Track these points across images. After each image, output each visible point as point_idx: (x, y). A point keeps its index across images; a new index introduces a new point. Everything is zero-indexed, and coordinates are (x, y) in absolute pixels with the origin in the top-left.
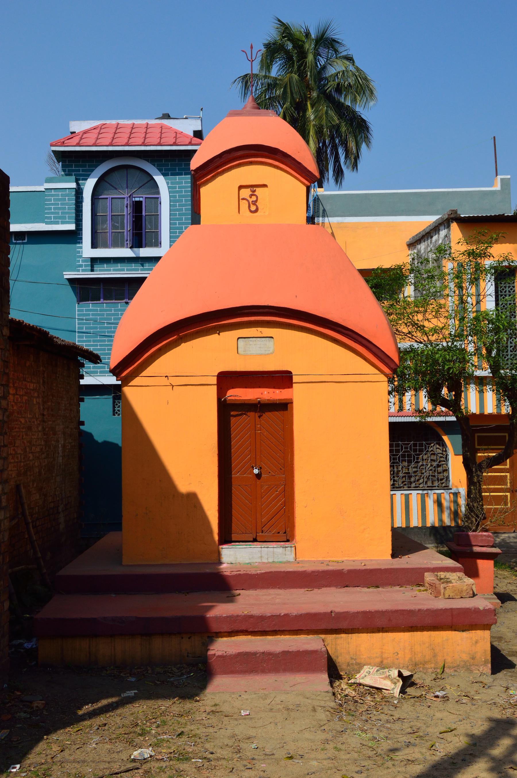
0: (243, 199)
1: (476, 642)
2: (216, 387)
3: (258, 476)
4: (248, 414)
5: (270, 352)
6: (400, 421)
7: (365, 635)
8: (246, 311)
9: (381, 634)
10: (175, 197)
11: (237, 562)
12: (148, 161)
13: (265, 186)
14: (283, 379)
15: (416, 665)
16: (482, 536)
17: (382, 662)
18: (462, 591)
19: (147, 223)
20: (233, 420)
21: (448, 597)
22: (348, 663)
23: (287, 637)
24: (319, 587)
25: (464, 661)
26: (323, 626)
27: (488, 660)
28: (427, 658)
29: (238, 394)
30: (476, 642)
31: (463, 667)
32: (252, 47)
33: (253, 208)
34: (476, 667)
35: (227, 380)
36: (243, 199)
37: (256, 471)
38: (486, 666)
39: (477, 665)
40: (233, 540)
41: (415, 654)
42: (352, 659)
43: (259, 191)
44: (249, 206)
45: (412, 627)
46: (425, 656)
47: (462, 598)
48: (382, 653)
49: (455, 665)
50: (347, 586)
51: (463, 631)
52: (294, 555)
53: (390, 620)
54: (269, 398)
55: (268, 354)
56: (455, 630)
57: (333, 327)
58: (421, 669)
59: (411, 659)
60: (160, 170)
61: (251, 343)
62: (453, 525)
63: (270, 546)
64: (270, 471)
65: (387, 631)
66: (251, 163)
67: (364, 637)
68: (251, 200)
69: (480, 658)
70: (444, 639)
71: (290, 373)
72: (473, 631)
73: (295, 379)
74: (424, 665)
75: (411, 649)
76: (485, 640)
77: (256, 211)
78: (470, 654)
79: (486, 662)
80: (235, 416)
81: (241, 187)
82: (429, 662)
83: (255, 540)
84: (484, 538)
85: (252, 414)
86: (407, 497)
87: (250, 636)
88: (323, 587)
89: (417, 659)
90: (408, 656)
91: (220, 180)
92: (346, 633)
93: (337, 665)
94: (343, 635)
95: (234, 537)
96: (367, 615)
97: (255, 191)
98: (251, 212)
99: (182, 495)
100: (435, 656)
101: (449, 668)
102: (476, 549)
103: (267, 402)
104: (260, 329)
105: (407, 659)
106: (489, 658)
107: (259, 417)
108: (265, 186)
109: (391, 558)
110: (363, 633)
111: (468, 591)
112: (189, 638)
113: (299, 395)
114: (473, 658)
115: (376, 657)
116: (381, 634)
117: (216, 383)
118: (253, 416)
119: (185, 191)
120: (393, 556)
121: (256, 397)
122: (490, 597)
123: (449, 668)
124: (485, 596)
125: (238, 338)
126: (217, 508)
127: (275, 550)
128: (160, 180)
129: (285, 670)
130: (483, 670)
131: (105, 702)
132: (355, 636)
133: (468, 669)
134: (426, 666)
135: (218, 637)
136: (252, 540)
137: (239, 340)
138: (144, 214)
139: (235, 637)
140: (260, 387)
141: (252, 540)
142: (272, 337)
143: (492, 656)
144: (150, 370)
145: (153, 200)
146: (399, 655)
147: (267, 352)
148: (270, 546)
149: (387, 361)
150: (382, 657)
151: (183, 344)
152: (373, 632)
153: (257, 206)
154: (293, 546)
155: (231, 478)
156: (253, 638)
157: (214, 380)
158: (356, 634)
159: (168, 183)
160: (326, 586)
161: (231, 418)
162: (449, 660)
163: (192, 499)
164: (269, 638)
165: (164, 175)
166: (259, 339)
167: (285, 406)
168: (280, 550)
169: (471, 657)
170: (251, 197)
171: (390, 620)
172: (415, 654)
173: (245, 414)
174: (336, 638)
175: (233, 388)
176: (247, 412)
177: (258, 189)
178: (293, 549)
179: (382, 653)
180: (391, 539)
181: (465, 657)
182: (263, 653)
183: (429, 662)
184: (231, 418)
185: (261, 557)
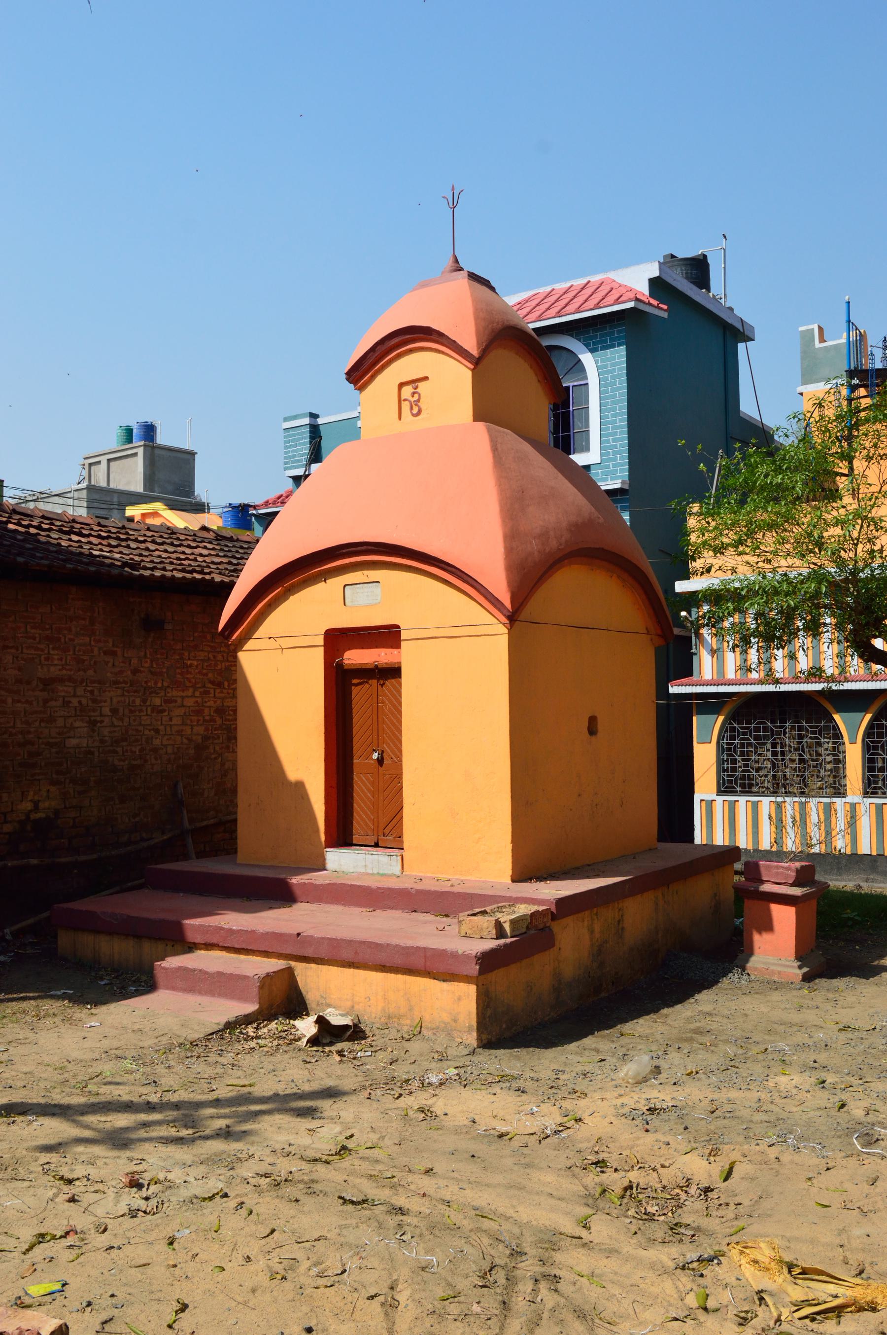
0: (405, 400)
1: (459, 999)
4: (370, 681)
5: (377, 601)
7: (335, 968)
10: (606, 379)
12: (572, 336)
14: (389, 635)
15: (389, 1017)
16: (777, 867)
17: (353, 1007)
19: (576, 420)
20: (355, 690)
25: (444, 1023)
29: (355, 657)
30: (459, 999)
31: (443, 1031)
32: (453, 189)
33: (415, 411)
35: (337, 640)
36: (405, 400)
42: (322, 997)
43: (421, 385)
44: (411, 408)
45: (384, 966)
48: (353, 995)
49: (434, 1026)
51: (444, 981)
53: (356, 953)
55: (376, 604)
59: (384, 1009)
60: (587, 345)
61: (358, 591)
65: (358, 968)
66: (411, 351)
68: (412, 400)
71: (398, 627)
72: (456, 983)
73: (404, 635)
74: (399, 1019)
77: (419, 412)
78: (451, 1013)
79: (470, 1027)
81: (401, 385)
83: (376, 845)
84: (781, 870)
85: (374, 682)
86: (755, 806)
89: (391, 1010)
91: (380, 379)
94: (313, 966)
95: (356, 839)
96: (335, 943)
97: (416, 388)
98: (414, 415)
99: (290, 783)
100: (411, 1009)
102: (766, 888)
103: (385, 666)
104: (366, 572)
105: (380, 1008)
107: (382, 685)
113: (407, 656)
114: (455, 1021)
118: (359, 682)
120: (518, 878)
122: (787, 963)
124: (780, 962)
125: (345, 586)
126: (323, 801)
127: (381, 858)
129: (220, 995)
131: (31, 995)
132: (325, 968)
134: (402, 1021)
135: (197, 949)
138: (571, 409)
140: (377, 647)
142: (378, 582)
143: (478, 1022)
144: (261, 632)
146: (371, 1002)
149: (496, 603)
152: (344, 966)
157: (320, 641)
159: (596, 362)
160: (392, 908)
162: (427, 1018)
163: (300, 786)
164: (242, 957)
166: (366, 585)
167: (394, 672)
168: (384, 859)
171: (356, 953)
174: (306, 968)
175: (349, 649)
177: (420, 384)
178: (399, 858)
179: (353, 995)
181: (446, 1017)
182: (200, 970)
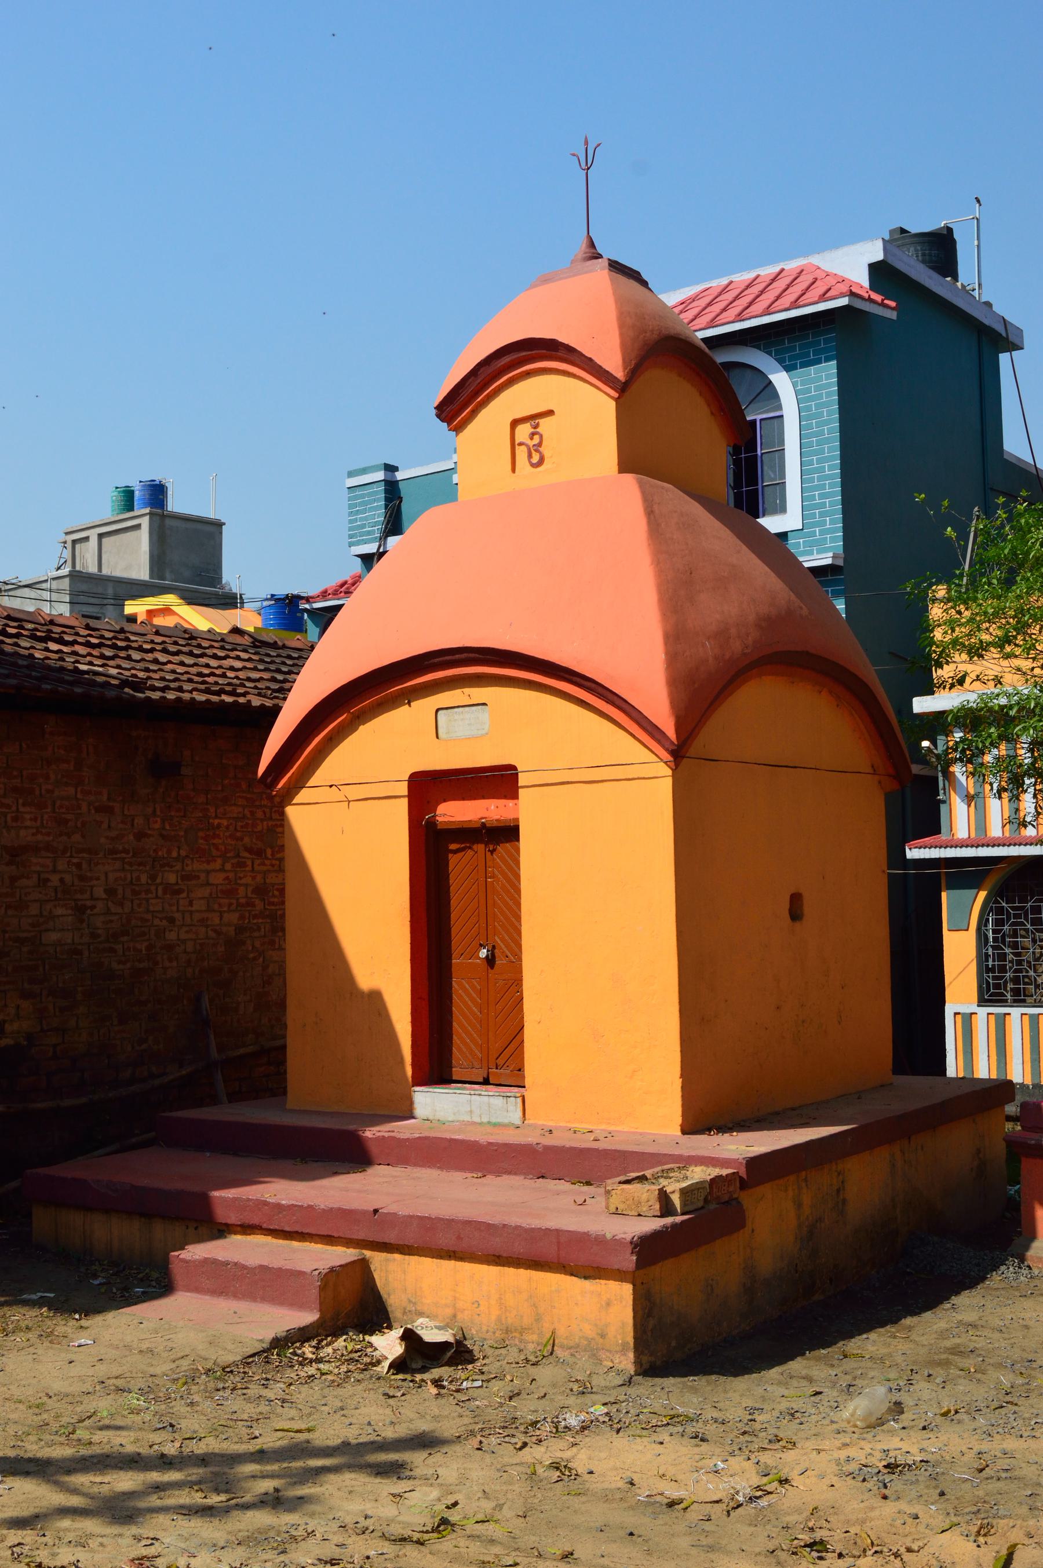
0: (520, 444)
1: (608, 1304)
2: (406, 800)
3: (490, 961)
4: (475, 847)
5: (484, 732)
6: (927, 857)
7: (429, 1260)
8: (436, 660)
9: (453, 1262)
11: (437, 1117)
13: (550, 413)
14: (501, 781)
15: (507, 1331)
17: (455, 1316)
18: (640, 1203)
19: (765, 468)
20: (453, 859)
21: (614, 1210)
22: (405, 1309)
23: (319, 1247)
24: (498, 1173)
25: (587, 1339)
26: (361, 1235)
27: (628, 1343)
28: (526, 1321)
29: (454, 812)
31: (585, 1350)
32: (586, 143)
33: (536, 458)
34: (608, 1354)
35: (427, 788)
36: (520, 444)
37: (483, 953)
38: (625, 1355)
39: (610, 1352)
40: (454, 1078)
41: (506, 1310)
42: (410, 1301)
44: (530, 456)
46: (522, 1317)
47: (639, 1215)
48: (455, 1298)
49: (571, 1343)
50: (543, 1177)
51: (586, 1278)
52: (520, 1113)
53: (459, 1238)
54: (498, 817)
55: (482, 735)
56: (572, 1275)
57: (567, 676)
58: (517, 1342)
59: (499, 1319)
60: (780, 361)
61: (456, 717)
62: (1028, 1081)
63: (483, 1093)
64: (509, 955)
66: (528, 374)
67: (427, 1264)
69: (615, 1337)
70: (553, 1289)
71: (513, 768)
72: (603, 1282)
73: (522, 780)
74: (521, 1334)
75: (501, 1299)
76: (624, 1303)
79: (624, 1345)
80: (455, 852)
81: (515, 423)
82: (529, 1329)
83: (486, 1082)
85: (480, 847)
86: (1001, 1022)
87: (270, 1237)
88: (505, 1173)
89: (510, 1321)
90: (495, 1313)
92: (401, 1253)
93: (389, 1309)
94: (397, 1256)
96: (428, 1224)
97: (536, 426)
98: (533, 465)
100: (538, 1319)
101: (562, 1347)
103: (495, 824)
105: (493, 1317)
106: (630, 1340)
107: (492, 852)
108: (550, 413)
109: (679, 1133)
110: (426, 1256)
111: (650, 1203)
112: (196, 1228)
113: (529, 810)
114: (603, 1336)
115: (446, 1305)
116: (452, 1263)
117: (520, 790)
119: (828, 395)
120: (690, 1128)
121: (479, 816)
123: (562, 1347)
125: (437, 711)
127: (492, 1099)
128: (781, 381)
130: (620, 1363)
133: (594, 1355)
136: (481, 1080)
137: (440, 712)
138: (759, 452)
139: (252, 1237)
140: (484, 798)
141: (481, 1080)
144: (323, 774)
145: (776, 421)
146: (481, 1308)
147: (480, 732)
148: (483, 1093)
150: (454, 1306)
151: (361, 727)
153: (540, 453)
154: (518, 1095)
155: (451, 964)
156: (275, 1241)
157: (403, 789)
158: (416, 1257)
159: (794, 385)
160: (510, 1173)
161: (450, 855)
163: (375, 997)
165: (788, 369)
166: (467, 709)
168: (498, 1102)
169: (599, 1332)
170: (532, 439)
172: (506, 1310)
173: (470, 848)
174: (387, 1260)
175: (445, 801)
176: (473, 844)
178: (519, 1100)
179: (455, 1298)
180: (680, 1094)
181: (589, 1331)
182: (236, 1264)
183: (529, 1329)
184: (450, 855)
185: (471, 1112)
